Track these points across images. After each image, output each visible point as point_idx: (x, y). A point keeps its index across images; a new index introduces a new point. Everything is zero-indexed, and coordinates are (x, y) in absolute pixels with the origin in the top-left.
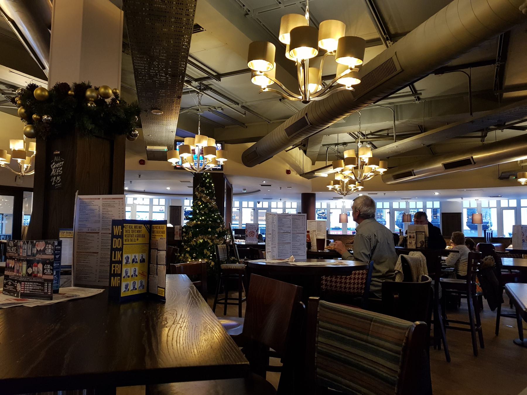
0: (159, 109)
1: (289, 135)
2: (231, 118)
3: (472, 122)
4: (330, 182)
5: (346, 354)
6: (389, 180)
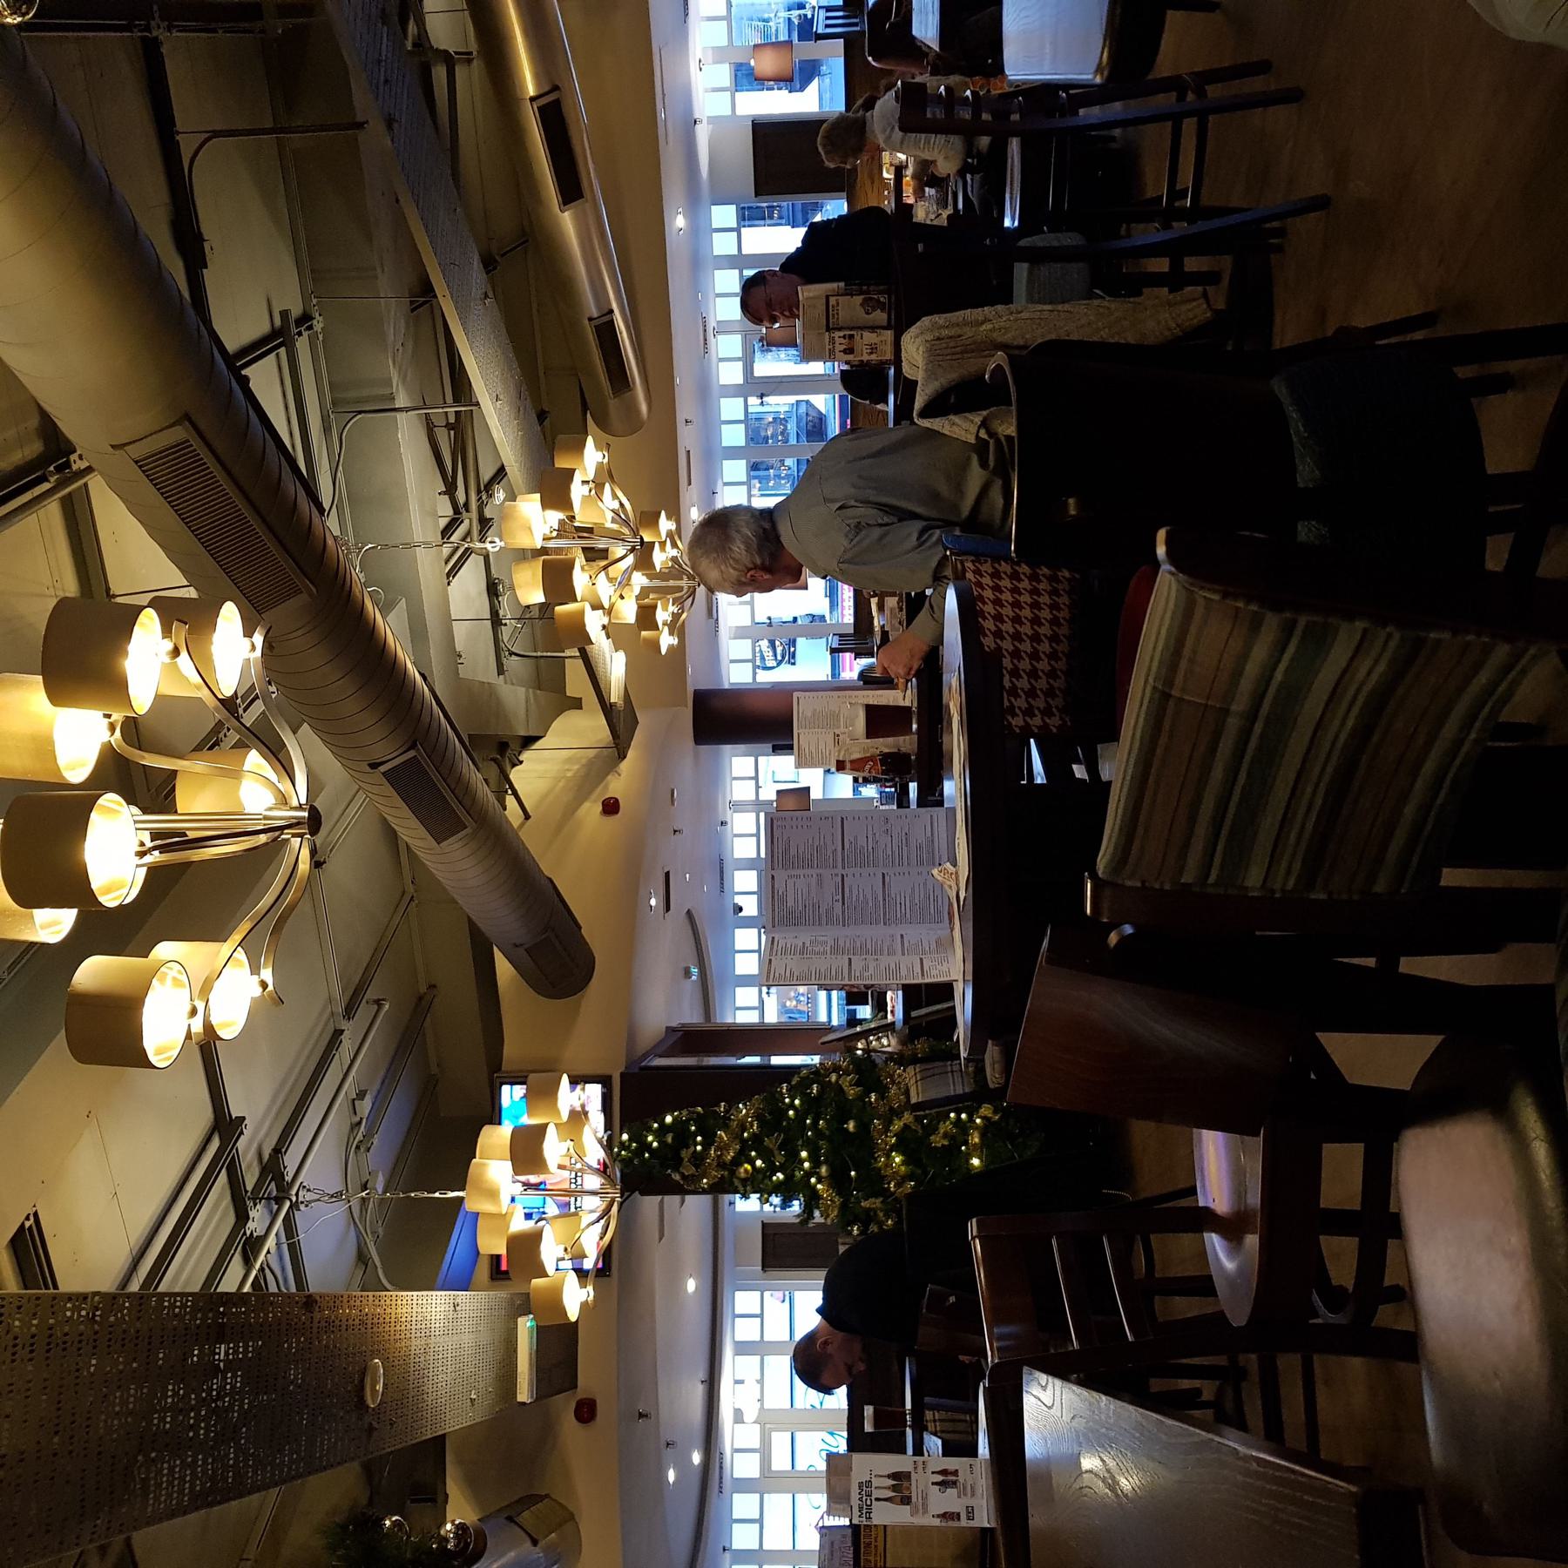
0: (362, 1381)
2: (396, 1054)
3: (390, 122)
4: (645, 640)
5: (1309, 790)
6: (632, 408)
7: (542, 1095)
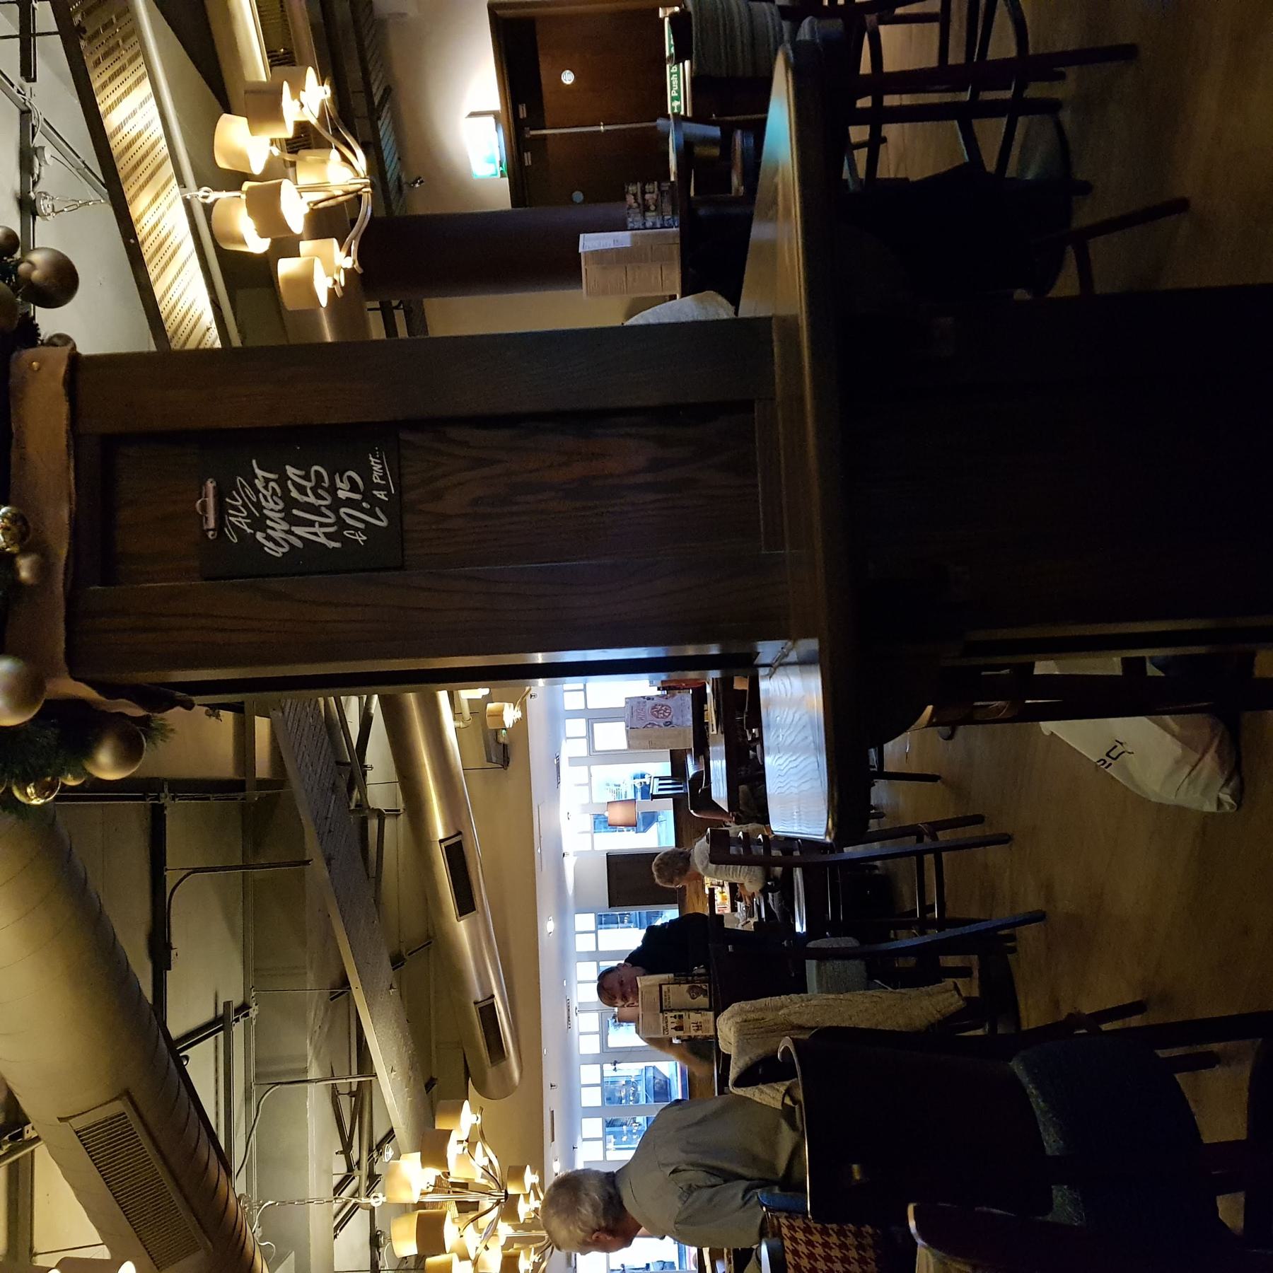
3: (329, 861)
6: (506, 1076)
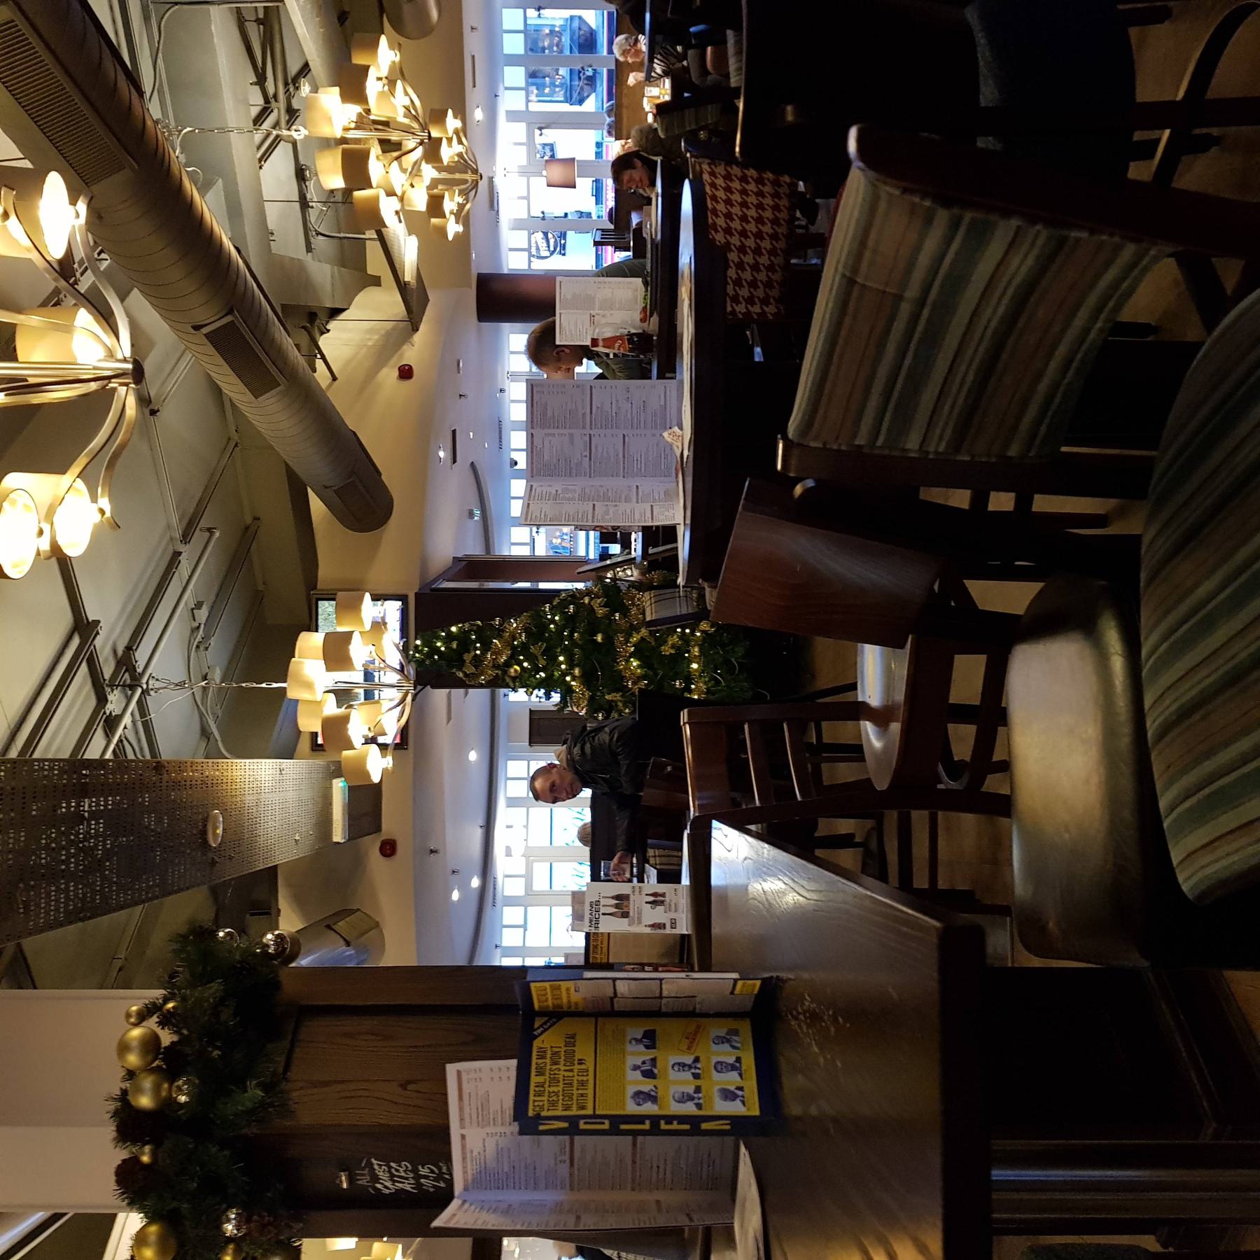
1: (274, 384)
7: (350, 608)
